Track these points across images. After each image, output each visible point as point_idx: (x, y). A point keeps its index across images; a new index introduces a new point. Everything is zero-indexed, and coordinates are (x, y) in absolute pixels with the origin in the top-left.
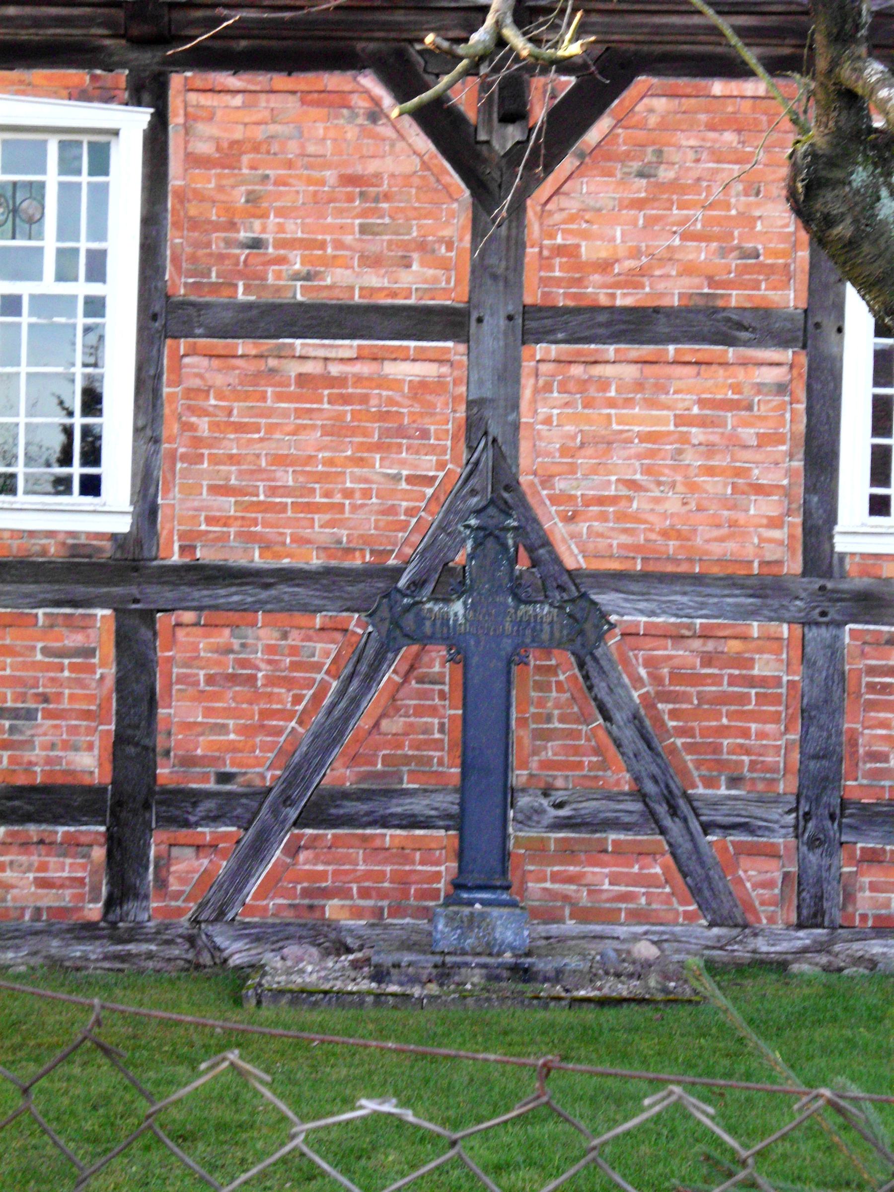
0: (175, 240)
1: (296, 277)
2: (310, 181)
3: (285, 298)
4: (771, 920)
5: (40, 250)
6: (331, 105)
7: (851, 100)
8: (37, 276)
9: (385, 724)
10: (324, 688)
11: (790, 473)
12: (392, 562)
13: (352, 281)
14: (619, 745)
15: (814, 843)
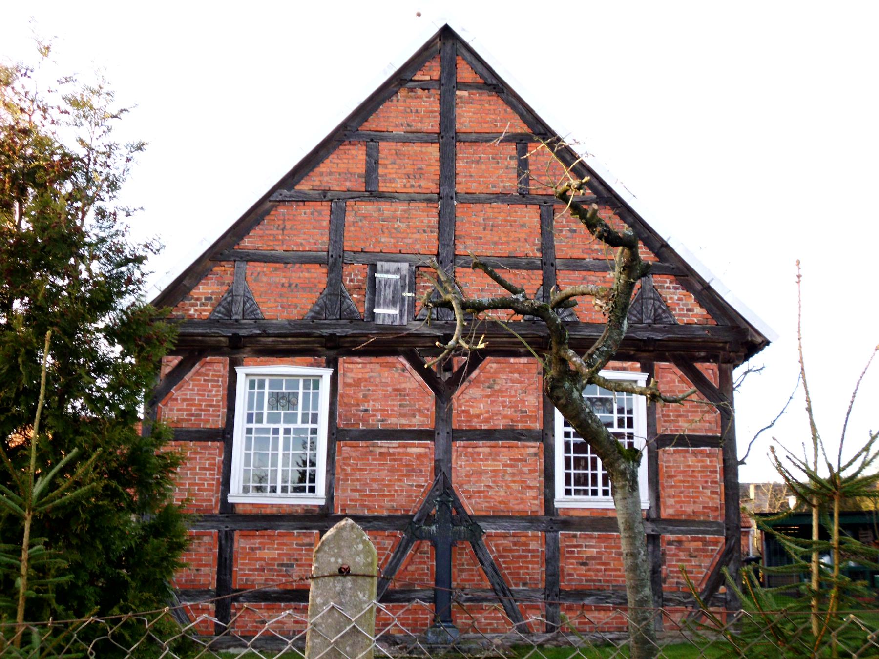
0: (340, 410)
1: (379, 421)
2: (383, 391)
3: (375, 428)
4: (538, 630)
5: (297, 414)
6: (390, 367)
7: (563, 361)
8: (296, 422)
9: (409, 568)
10: (388, 555)
11: (539, 482)
12: (411, 513)
13: (397, 422)
14: (486, 573)
15: (550, 605)
